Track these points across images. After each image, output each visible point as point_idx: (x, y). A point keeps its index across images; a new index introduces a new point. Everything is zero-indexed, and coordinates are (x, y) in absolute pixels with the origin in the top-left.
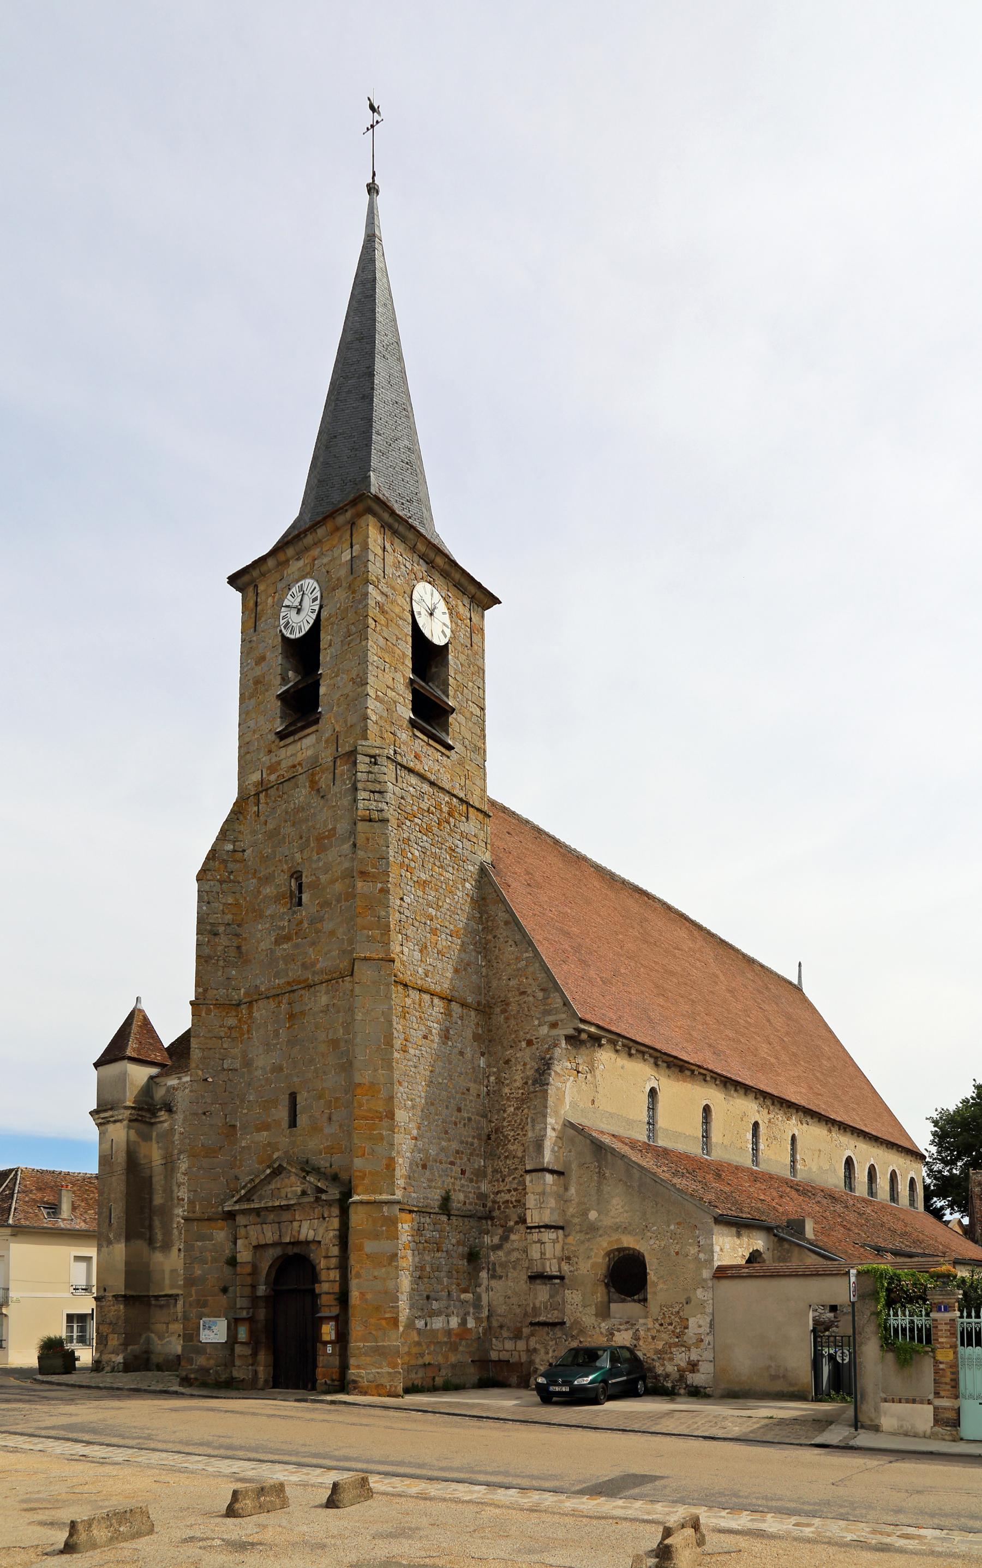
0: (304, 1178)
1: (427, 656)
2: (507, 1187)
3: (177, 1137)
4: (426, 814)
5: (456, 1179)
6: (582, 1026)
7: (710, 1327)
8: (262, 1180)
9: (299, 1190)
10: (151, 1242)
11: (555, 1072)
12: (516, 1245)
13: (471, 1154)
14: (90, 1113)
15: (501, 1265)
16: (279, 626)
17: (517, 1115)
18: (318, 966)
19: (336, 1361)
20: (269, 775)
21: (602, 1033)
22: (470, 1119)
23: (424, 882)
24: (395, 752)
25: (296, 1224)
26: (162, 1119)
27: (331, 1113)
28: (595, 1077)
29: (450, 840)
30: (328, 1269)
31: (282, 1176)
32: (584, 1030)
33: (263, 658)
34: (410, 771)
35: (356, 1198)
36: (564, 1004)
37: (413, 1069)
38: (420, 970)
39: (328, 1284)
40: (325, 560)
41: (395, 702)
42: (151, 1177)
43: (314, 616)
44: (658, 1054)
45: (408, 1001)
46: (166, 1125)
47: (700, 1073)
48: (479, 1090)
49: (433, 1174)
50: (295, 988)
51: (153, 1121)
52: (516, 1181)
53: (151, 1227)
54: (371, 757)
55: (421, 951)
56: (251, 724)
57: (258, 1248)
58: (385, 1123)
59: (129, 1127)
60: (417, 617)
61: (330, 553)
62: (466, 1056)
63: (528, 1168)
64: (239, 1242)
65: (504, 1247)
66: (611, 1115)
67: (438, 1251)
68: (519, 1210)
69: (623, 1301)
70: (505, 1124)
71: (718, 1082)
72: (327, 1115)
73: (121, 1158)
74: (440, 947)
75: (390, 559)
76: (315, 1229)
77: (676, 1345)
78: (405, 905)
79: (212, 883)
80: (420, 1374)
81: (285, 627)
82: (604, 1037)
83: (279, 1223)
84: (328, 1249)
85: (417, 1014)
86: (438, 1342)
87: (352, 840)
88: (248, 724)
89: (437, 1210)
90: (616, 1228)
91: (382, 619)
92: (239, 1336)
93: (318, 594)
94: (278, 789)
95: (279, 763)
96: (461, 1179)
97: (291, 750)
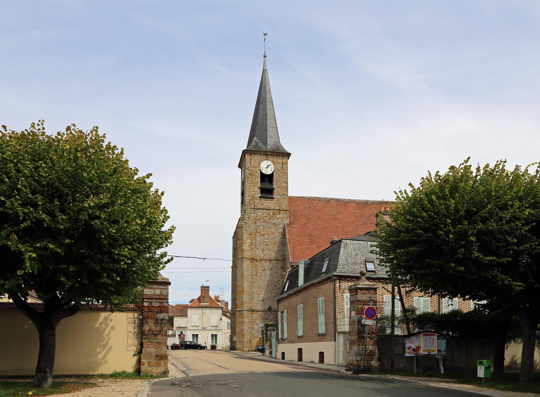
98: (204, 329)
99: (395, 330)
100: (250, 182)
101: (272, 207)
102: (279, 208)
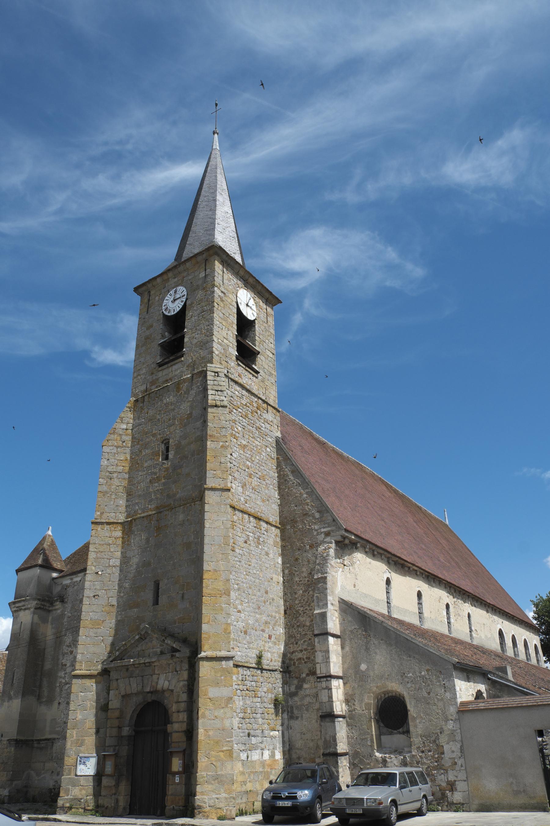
0: (164, 640)
1: (244, 326)
2: (300, 648)
3: (65, 620)
4: (245, 407)
5: (265, 642)
6: (347, 534)
7: (461, 752)
8: (132, 644)
9: (159, 650)
10: (39, 698)
11: (331, 564)
12: (308, 692)
13: (275, 625)
14: (9, 604)
15: (297, 708)
16: (162, 310)
17: (305, 596)
18: (178, 496)
19: (182, 789)
20: (151, 386)
21: (358, 540)
23: (244, 445)
24: (228, 372)
25: (155, 677)
26: (57, 607)
27: (183, 594)
28: (354, 569)
29: (259, 423)
30: (178, 712)
31: (146, 641)
32: (347, 537)
33: (151, 326)
34: (236, 382)
35: (203, 654)
36: (334, 520)
37: (238, 563)
38: (242, 499)
39: (177, 727)
40: (190, 278)
41: (228, 346)
42: (44, 649)
43: (183, 304)
44: (390, 556)
45: (235, 518)
46: (59, 611)
47: (414, 570)
48: (278, 579)
50: (162, 510)
51: (50, 609)
52: (306, 643)
53: (40, 687)
54: (215, 372)
55: (242, 487)
56: (142, 360)
57: (125, 697)
58: (224, 598)
59: (34, 613)
60: (239, 305)
61: (193, 274)
62: (270, 556)
63: (316, 632)
64: (111, 692)
65: (299, 693)
66: (366, 596)
67: (255, 697)
68: (310, 665)
69: (391, 734)
70: (297, 602)
71: (424, 576)
72: (181, 595)
73: (26, 635)
74: (253, 485)
75: (226, 277)
76: (168, 681)
77: (435, 768)
78: (233, 458)
80: (244, 800)
81: (165, 310)
82: (359, 542)
83: (142, 676)
84: (178, 696)
85: (241, 526)
86: (256, 772)
87: (202, 419)
88: (140, 360)
89: (254, 665)
90: (381, 677)
91: (222, 305)
92: (106, 769)
93: (186, 293)
94: (156, 393)
95: (157, 379)
97: (165, 372)
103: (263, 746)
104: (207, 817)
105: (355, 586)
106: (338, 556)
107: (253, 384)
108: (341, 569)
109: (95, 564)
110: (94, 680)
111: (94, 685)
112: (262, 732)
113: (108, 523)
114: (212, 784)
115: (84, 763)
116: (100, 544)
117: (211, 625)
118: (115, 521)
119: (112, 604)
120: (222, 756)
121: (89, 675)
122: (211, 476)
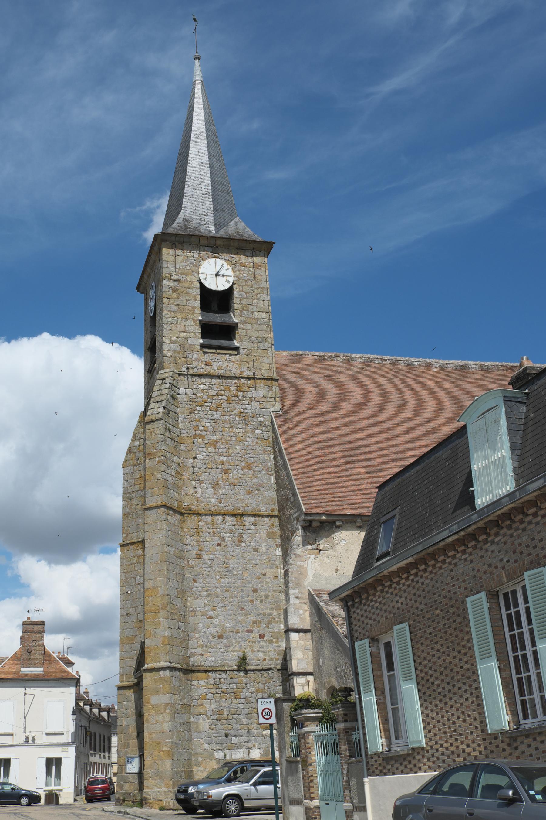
22: (267, 596)
23: (216, 441)
35: (146, 666)
49: (230, 642)
67: (236, 698)
79: (129, 468)
96: (259, 642)
98: (29, 742)
99: (269, 733)
100: (174, 308)
101: (235, 372)
102: (251, 374)
103: (250, 745)
104: (152, 807)
105: (337, 571)
106: (306, 542)
107: (231, 365)
108: (313, 556)
109: (125, 584)
110: (132, 690)
111: (133, 694)
112: (249, 731)
113: (132, 544)
114: (155, 780)
115: (131, 763)
116: (127, 565)
117: (152, 639)
118: (136, 540)
119: (140, 619)
120: (163, 756)
121: (128, 686)
122: (150, 495)
